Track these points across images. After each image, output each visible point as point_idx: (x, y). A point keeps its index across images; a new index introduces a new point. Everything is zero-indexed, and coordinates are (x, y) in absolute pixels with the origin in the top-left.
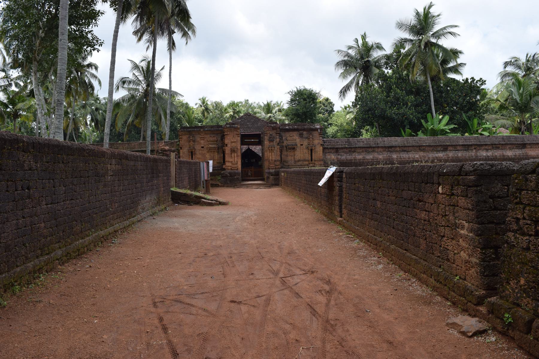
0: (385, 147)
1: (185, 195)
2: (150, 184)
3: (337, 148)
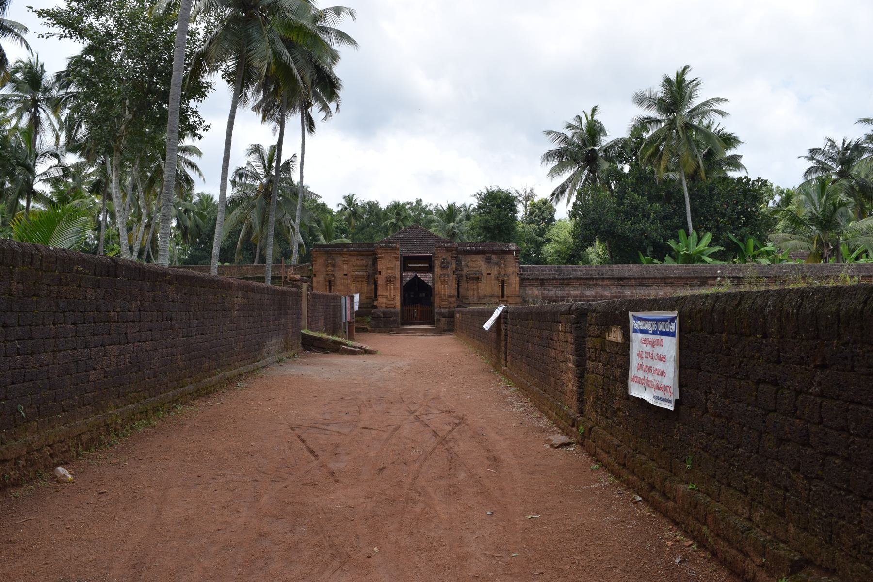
0: (613, 279)
1: (320, 339)
2: (276, 323)
3: (542, 280)
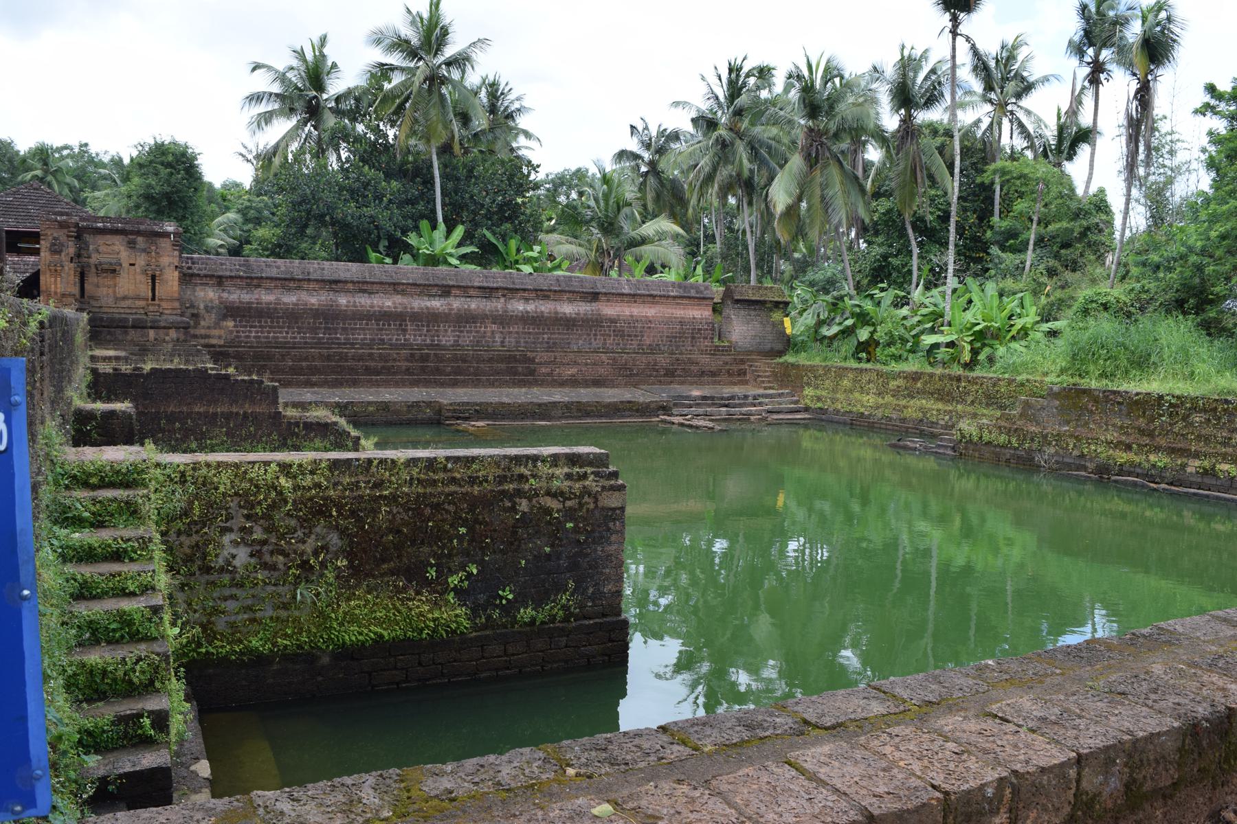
0: (323, 281)
3: (220, 277)
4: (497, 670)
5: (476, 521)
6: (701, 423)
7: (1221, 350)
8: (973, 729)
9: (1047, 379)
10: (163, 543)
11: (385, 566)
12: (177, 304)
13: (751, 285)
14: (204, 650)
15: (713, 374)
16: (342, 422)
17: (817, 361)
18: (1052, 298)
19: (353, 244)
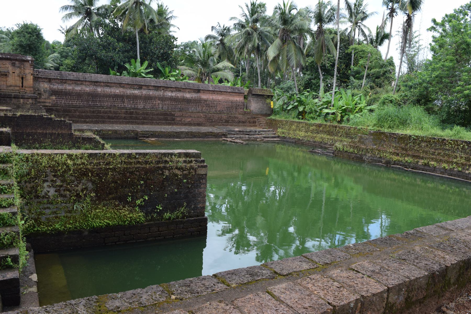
0: (91, 81)
3: (50, 79)
4: (155, 237)
5: (148, 179)
6: (238, 141)
7: (433, 119)
8: (345, 276)
9: (369, 128)
10: (18, 186)
11: (111, 196)
12: (32, 89)
13: (259, 88)
14: (36, 229)
15: (243, 122)
16: (98, 137)
17: (283, 119)
18: (372, 97)
19: (104, 67)
